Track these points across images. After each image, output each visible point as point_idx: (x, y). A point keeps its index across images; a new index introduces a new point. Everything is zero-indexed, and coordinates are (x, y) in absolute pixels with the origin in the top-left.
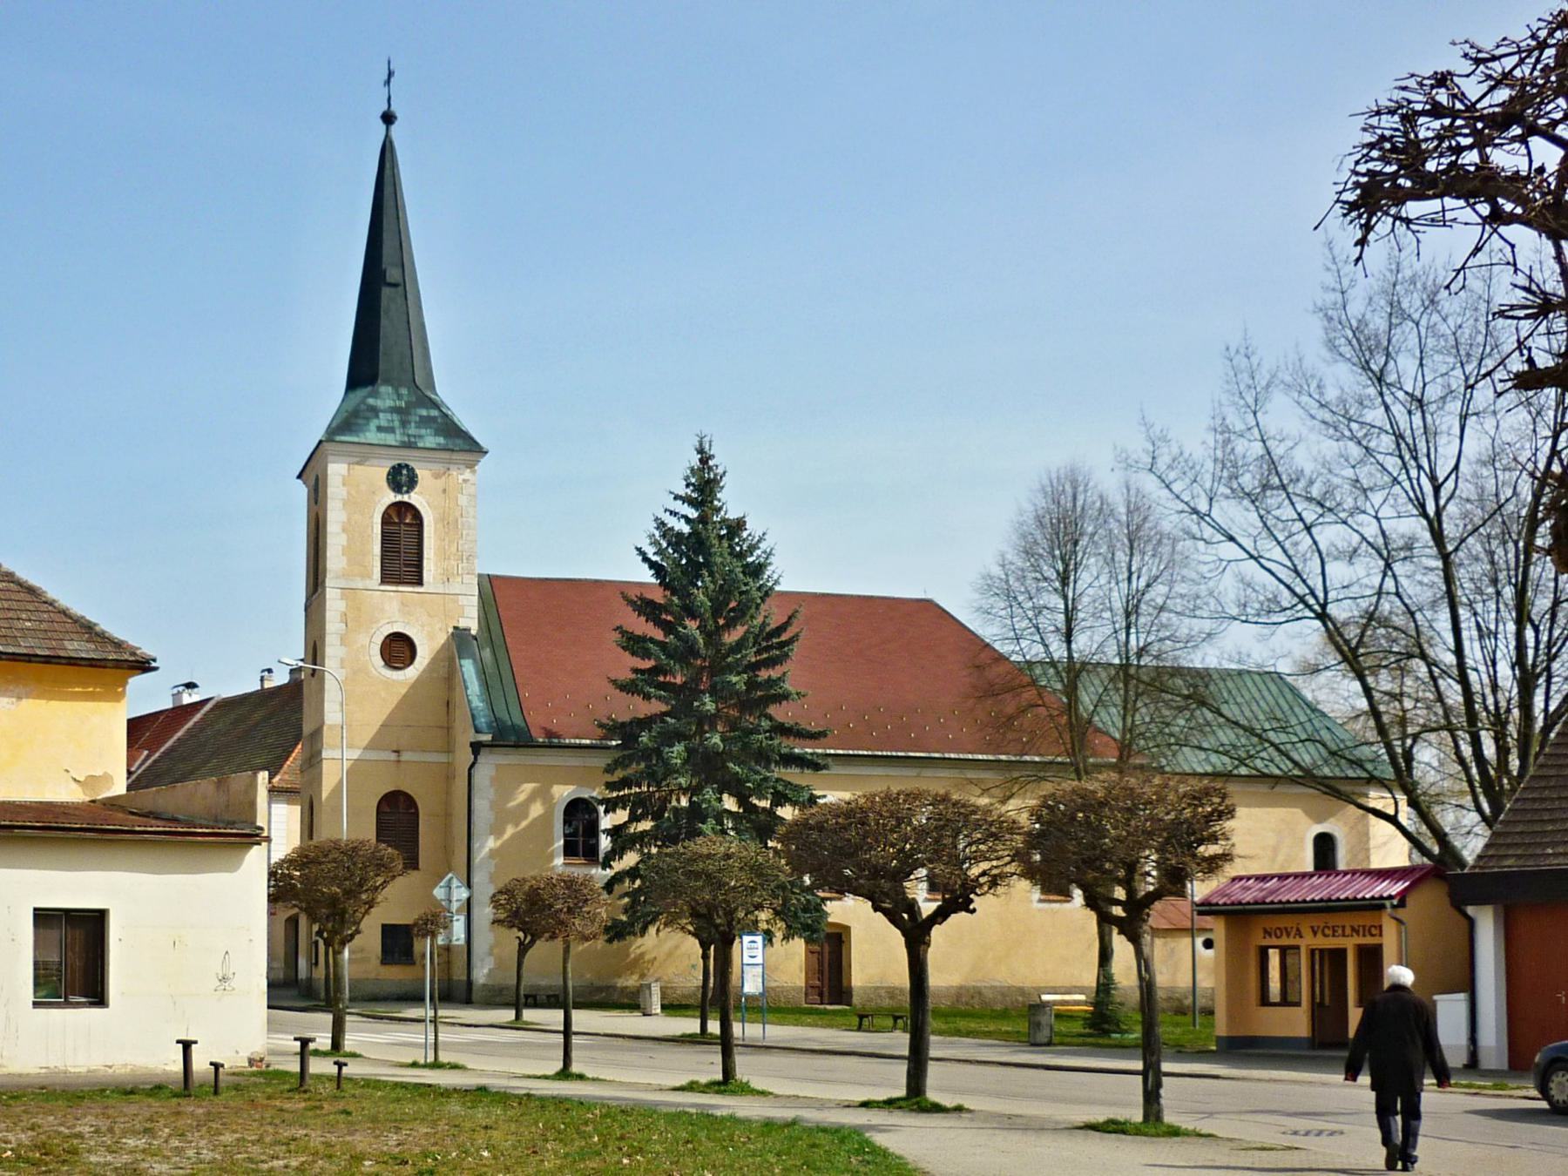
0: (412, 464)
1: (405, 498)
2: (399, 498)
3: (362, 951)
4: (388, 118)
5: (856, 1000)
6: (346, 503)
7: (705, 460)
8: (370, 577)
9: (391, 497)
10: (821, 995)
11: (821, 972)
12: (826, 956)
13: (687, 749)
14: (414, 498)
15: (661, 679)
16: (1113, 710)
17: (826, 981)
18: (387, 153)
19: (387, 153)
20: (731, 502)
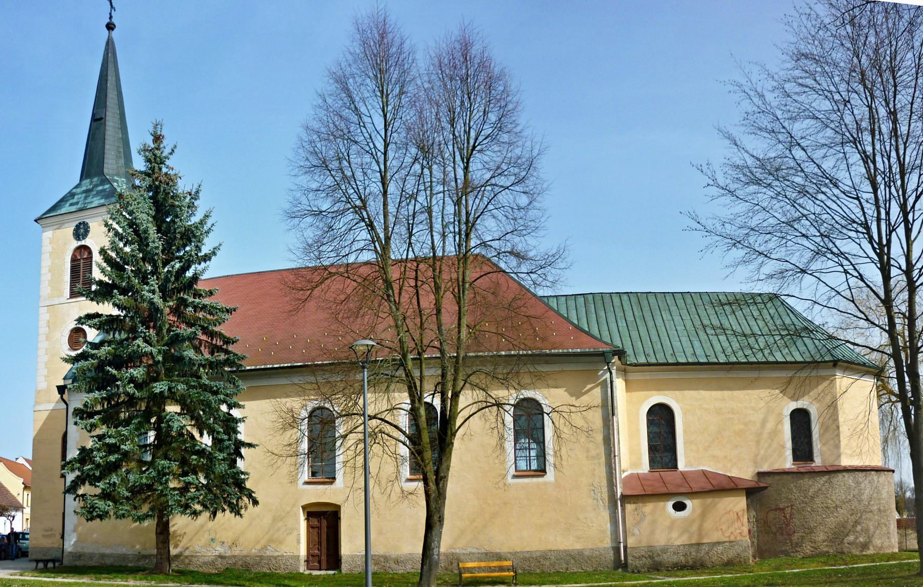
0: (86, 221)
1: (83, 243)
2: (80, 243)
3: (51, 530)
4: (110, 27)
5: (345, 568)
6: (51, 254)
7: (157, 138)
8: (61, 295)
9: (76, 244)
10: (320, 562)
11: (320, 543)
12: (324, 530)
13: (159, 361)
14: (87, 242)
15: (909, 395)
16: (783, 254)
17: (324, 551)
18: (110, 44)
19: (110, 44)
20: (174, 164)
